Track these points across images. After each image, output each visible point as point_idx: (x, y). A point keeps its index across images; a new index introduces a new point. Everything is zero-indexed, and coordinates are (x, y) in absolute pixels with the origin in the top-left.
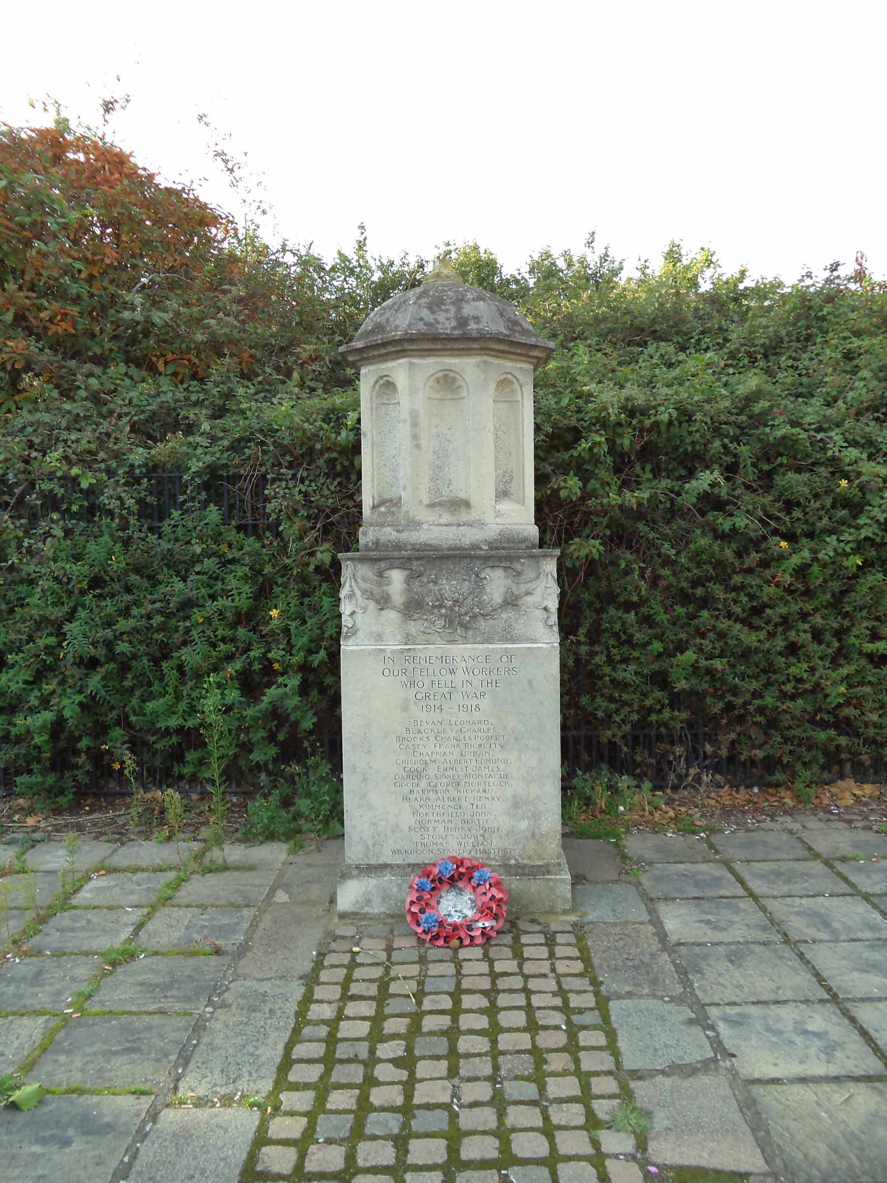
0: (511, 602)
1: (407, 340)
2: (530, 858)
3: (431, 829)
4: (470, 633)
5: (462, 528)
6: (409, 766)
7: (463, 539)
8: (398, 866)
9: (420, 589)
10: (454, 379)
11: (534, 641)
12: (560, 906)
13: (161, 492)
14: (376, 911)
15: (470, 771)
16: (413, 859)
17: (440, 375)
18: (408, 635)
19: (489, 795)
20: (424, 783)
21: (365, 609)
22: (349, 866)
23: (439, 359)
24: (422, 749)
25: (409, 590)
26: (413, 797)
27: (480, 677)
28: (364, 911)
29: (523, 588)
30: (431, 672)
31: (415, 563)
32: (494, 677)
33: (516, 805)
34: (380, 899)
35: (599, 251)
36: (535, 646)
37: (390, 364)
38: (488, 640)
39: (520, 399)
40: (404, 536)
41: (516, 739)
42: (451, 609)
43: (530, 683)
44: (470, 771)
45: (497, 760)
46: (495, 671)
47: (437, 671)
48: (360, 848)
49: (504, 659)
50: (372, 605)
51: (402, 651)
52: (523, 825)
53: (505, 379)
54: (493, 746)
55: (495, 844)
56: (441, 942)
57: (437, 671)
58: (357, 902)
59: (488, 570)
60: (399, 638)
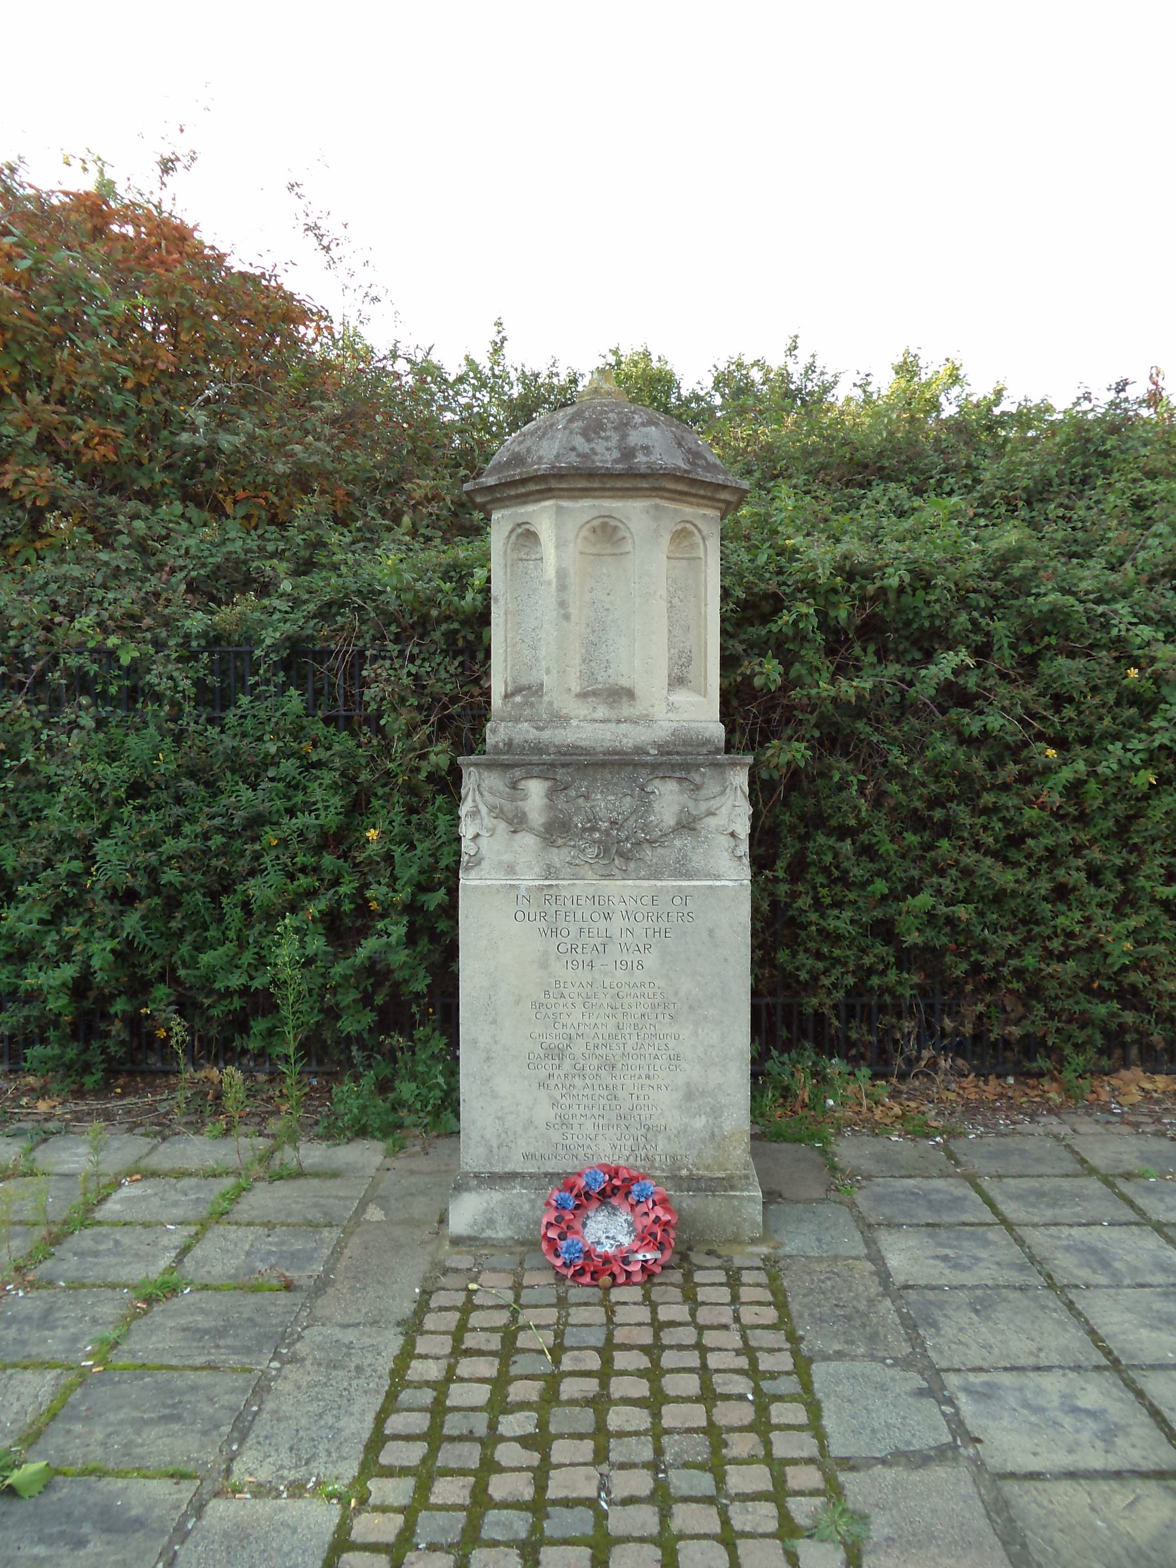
0: (687, 825)
1: (554, 476)
2: (707, 1168)
3: (576, 1126)
4: (632, 865)
5: (623, 726)
6: (548, 1041)
7: (625, 740)
8: (531, 1175)
9: (565, 806)
10: (615, 528)
11: (717, 877)
12: (748, 1233)
13: (225, 670)
14: (501, 1235)
15: (628, 1049)
16: (551, 1167)
17: (596, 523)
18: (549, 866)
19: (653, 1083)
20: (567, 1064)
21: (492, 832)
22: (466, 1174)
23: (597, 502)
24: (564, 1019)
25: (551, 806)
26: (552, 1082)
27: (645, 924)
28: (484, 1235)
29: (703, 806)
30: (579, 916)
31: (560, 771)
32: (663, 924)
33: (689, 1096)
34: (506, 1219)
35: (803, 357)
36: (718, 883)
37: (531, 508)
38: (655, 875)
39: (702, 555)
40: (546, 735)
41: (690, 1007)
42: (607, 833)
43: (711, 932)
44: (628, 1049)
45: (666, 1036)
46: (665, 917)
47: (587, 916)
48: (481, 1150)
49: (677, 901)
50: (502, 826)
51: (541, 888)
52: (700, 1123)
53: (684, 529)
54: (660, 1017)
55: (662, 1147)
56: (587, 1279)
57: (587, 916)
58: (475, 1223)
59: (657, 782)
60: (537, 870)
